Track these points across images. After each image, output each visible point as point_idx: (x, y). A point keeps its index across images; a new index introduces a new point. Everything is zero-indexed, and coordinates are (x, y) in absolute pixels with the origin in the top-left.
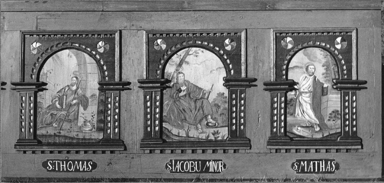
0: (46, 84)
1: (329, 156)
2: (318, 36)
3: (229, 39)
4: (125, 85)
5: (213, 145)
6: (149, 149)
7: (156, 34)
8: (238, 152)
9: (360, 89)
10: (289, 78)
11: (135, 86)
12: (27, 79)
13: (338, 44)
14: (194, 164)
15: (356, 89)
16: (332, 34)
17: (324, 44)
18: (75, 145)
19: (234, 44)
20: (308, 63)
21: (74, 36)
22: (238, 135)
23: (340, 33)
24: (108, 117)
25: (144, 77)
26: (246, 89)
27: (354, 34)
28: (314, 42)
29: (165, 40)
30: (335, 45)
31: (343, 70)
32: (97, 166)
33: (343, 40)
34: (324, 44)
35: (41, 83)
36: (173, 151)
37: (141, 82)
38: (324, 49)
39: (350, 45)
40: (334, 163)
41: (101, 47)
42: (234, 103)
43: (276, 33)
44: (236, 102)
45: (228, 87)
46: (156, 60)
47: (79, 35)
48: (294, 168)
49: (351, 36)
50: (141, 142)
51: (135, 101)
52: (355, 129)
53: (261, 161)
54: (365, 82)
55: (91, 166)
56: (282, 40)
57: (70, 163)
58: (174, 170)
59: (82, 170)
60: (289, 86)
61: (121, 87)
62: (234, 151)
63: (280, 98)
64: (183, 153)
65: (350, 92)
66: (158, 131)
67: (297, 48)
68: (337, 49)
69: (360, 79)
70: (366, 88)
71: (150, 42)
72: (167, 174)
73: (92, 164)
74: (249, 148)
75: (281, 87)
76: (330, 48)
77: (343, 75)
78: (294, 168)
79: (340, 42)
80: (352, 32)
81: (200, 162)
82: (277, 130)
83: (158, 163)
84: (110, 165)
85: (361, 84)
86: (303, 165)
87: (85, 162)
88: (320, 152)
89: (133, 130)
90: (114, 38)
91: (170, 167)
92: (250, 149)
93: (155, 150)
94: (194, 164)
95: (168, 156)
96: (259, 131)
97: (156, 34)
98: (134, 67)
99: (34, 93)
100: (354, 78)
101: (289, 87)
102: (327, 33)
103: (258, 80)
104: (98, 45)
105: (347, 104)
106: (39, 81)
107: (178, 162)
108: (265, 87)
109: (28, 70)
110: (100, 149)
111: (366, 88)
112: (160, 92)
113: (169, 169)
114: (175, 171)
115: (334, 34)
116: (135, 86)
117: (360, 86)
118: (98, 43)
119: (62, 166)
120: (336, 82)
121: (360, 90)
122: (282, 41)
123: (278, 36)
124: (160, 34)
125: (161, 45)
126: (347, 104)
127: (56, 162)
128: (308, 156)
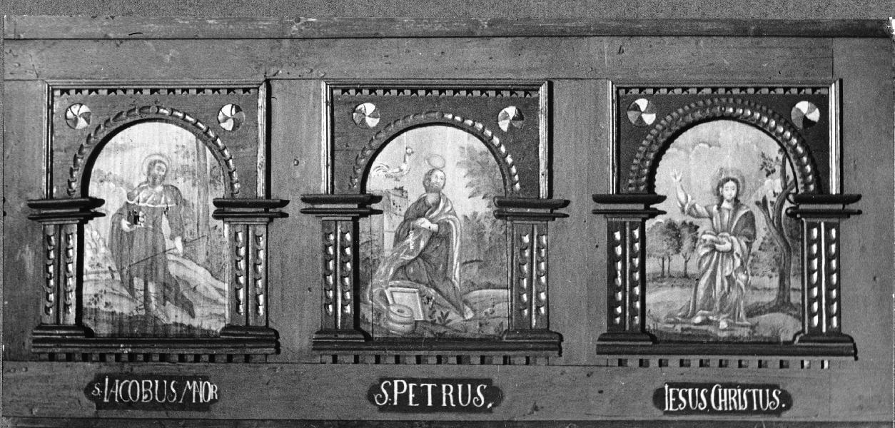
0: (101, 202)
3: (230, 106)
4: (554, 209)
7: (688, 88)
9: (848, 214)
14: (151, 385)
15: (546, 219)
17: (450, 116)
18: (174, 342)
20: (160, 155)
21: (135, 92)
23: (641, 89)
24: (328, 277)
25: (322, 188)
29: (658, 106)
30: (497, 121)
31: (511, 176)
32: (790, 396)
34: (450, 116)
41: (226, 119)
42: (638, 249)
43: (618, 89)
47: (411, 90)
51: (579, 240)
53: (579, 379)
54: (858, 198)
55: (780, 399)
60: (80, 209)
63: (538, 237)
64: (199, 362)
65: (822, 224)
67: (677, 125)
70: (860, 212)
71: (623, 104)
72: (88, 409)
76: (473, 125)
77: (806, 185)
83: (631, 388)
85: (557, 209)
86: (190, 388)
90: (537, 100)
91: (387, 396)
94: (151, 385)
95: (370, 371)
97: (688, 88)
98: (580, 161)
100: (834, 190)
102: (739, 90)
103: (668, 197)
104: (221, 113)
105: (815, 248)
107: (188, 383)
112: (351, 223)
115: (668, 92)
116: (581, 206)
118: (221, 109)
121: (849, 217)
123: (338, 96)
124: (61, 89)
126: (815, 248)
127: (426, 387)
128: (441, 371)
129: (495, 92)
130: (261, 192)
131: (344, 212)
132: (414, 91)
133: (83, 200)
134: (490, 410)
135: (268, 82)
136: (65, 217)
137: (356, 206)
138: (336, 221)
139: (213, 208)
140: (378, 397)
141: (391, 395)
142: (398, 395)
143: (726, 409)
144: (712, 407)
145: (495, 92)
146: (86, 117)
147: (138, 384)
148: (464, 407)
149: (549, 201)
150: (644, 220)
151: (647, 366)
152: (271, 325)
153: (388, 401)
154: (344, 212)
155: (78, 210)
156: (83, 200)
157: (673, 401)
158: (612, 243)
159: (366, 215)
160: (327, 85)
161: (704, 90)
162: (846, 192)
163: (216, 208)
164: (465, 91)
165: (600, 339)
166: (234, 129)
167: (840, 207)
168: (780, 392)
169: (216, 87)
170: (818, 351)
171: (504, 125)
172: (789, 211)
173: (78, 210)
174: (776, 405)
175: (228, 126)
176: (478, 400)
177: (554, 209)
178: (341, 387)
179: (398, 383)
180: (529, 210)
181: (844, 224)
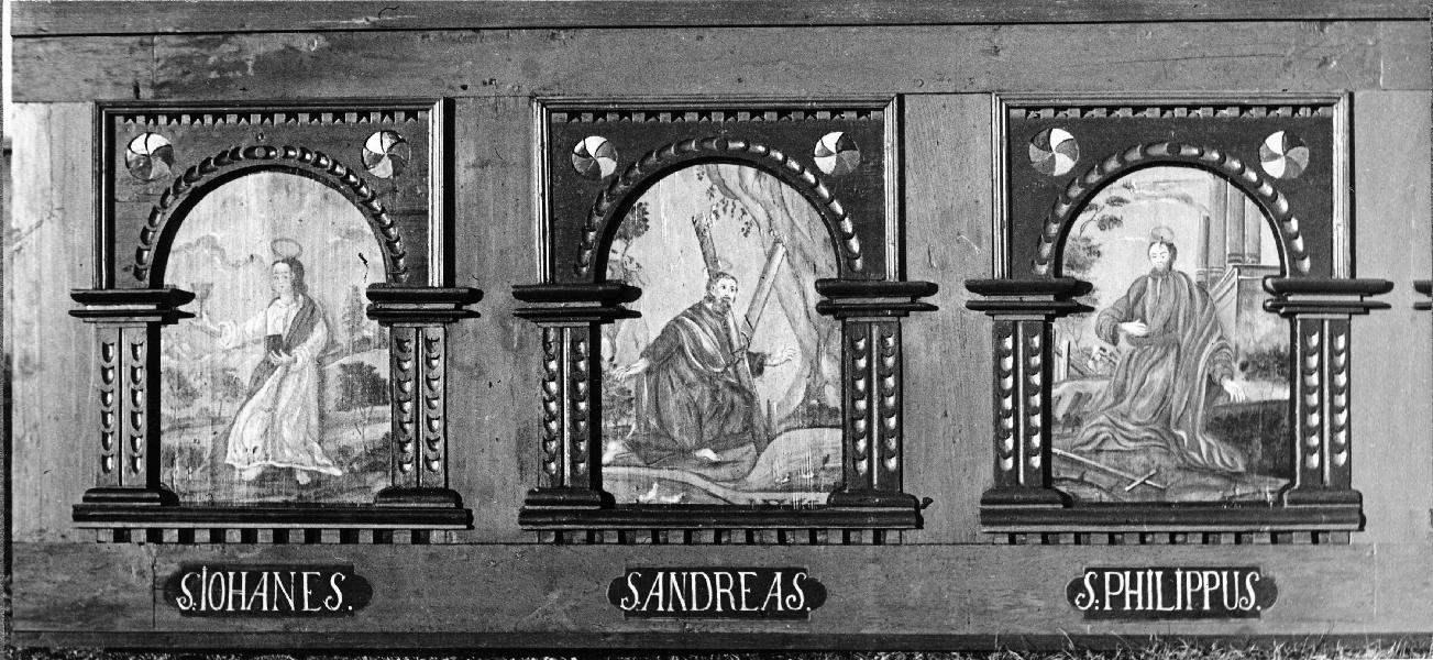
1: (1243, 555)
2: (1091, 120)
3: (377, 135)
5: (1173, 519)
6: (1106, 529)
8: (1290, 542)
9: (1366, 309)
10: (168, 280)
11: (952, 299)
12: (125, 281)
13: (1274, 156)
16: (1263, 113)
19: (1302, 155)
22: (875, 482)
26: (1350, 318)
27: (1339, 115)
28: (1175, 147)
29: (619, 141)
33: (844, 144)
35: (168, 291)
36: (779, 539)
37: (521, 293)
38: (1217, 170)
39: (1321, 162)
40: (1253, 577)
44: (881, 363)
45: (1282, 311)
46: (1039, 210)
48: (1077, 602)
49: (1330, 120)
50: (528, 502)
52: (892, 463)
56: (1032, 141)
57: (218, 576)
58: (246, 606)
59: (249, 608)
61: (452, 306)
62: (1110, 538)
66: (1037, 471)
68: (1271, 180)
69: (1363, 274)
70: (1387, 306)
72: (616, 625)
73: (1257, 579)
74: (1357, 526)
75: (572, 305)
78: (1077, 602)
79: (1280, 152)
80: (883, 110)
81: (244, 574)
82: (1016, 463)
84: (866, 587)
85: (1371, 295)
87: (779, 575)
88: (1122, 542)
89: (953, 469)
92: (1361, 528)
93: (885, 530)
96: (953, 469)
99: (590, 327)
100: (1340, 271)
101: (602, 306)
102: (748, 114)
106: (161, 285)
108: (521, 304)
109: (125, 254)
110: (236, 525)
111: (1387, 306)
113: (1084, 602)
114: (249, 608)
117: (1366, 299)
119: (1131, 596)
120: (1274, 285)
122: (1032, 147)
125: (599, 160)
129: (1211, 109)
130: (436, 277)
131: (1034, 309)
132: (339, 115)
133: (446, 290)
134: (803, 614)
135: (901, 98)
136: (417, 315)
137: (1051, 298)
138: (870, 323)
139: (814, 298)
140: (791, 599)
141: (1100, 594)
142: (1192, 593)
143: (1140, 607)
144: (1222, 603)
145: (1291, 108)
146: (166, 154)
147: (1199, 576)
148: (1227, 610)
149: (1353, 281)
150: (1050, 318)
151: (389, 541)
152: (451, 486)
153: (1094, 605)
154: (1034, 309)
155: (452, 306)
156: (446, 290)
157: (746, 593)
158: (1000, 355)
159: (1063, 312)
160: (1001, 101)
161: (1253, 111)
162: (1361, 275)
163: (370, 302)
164: (403, 114)
165: (984, 502)
166: (396, 173)
167: (1356, 298)
168: (1257, 579)
169: (1168, 102)
170: (554, 517)
171: (827, 165)
172: (1269, 304)
173: (599, 305)
174: (1248, 605)
175: (384, 170)
176: (795, 599)
177: (460, 301)
178: (569, 596)
179: (721, 576)
180: (563, 305)
181: (1358, 322)
